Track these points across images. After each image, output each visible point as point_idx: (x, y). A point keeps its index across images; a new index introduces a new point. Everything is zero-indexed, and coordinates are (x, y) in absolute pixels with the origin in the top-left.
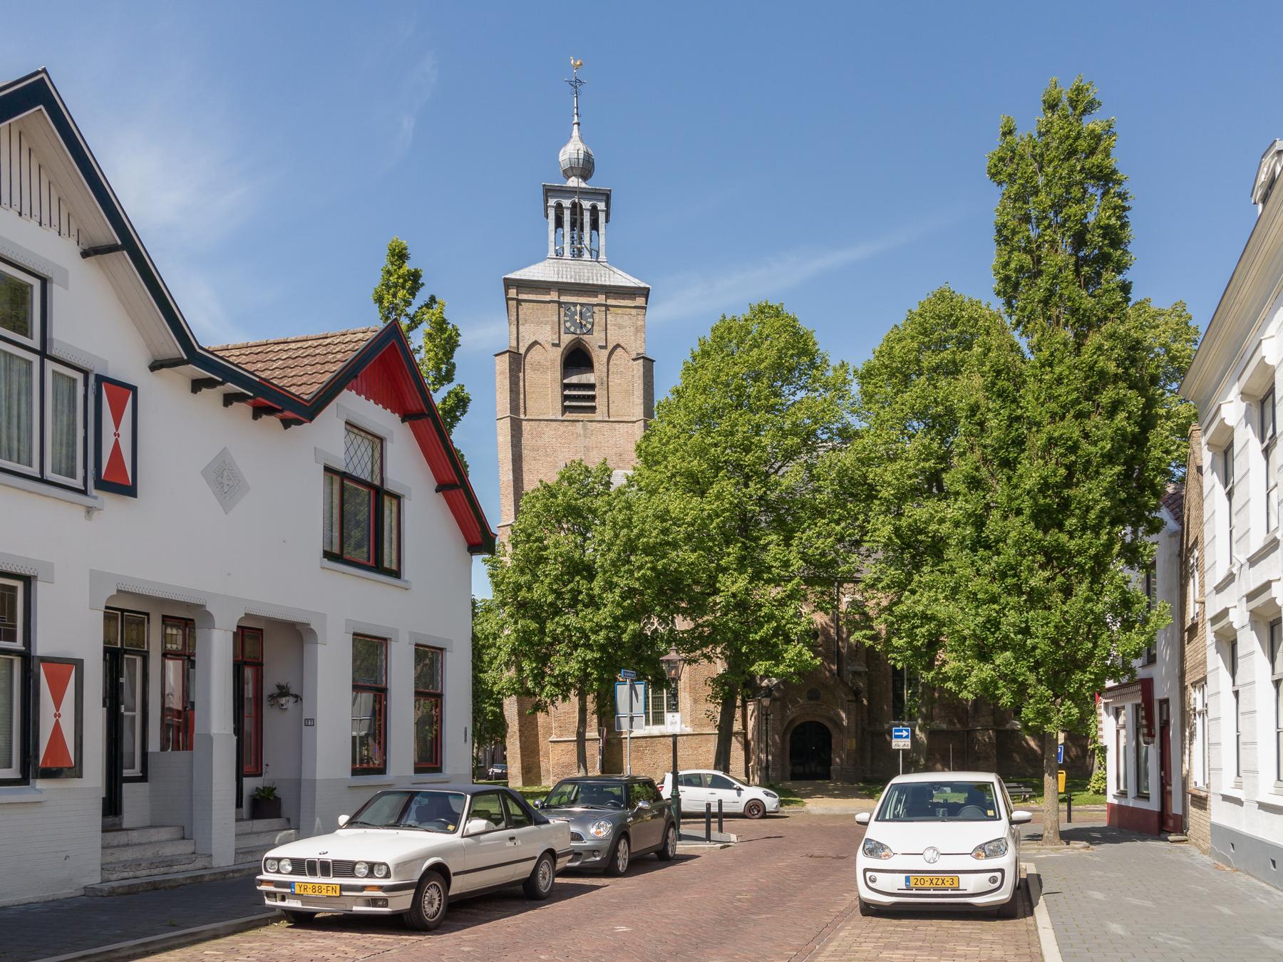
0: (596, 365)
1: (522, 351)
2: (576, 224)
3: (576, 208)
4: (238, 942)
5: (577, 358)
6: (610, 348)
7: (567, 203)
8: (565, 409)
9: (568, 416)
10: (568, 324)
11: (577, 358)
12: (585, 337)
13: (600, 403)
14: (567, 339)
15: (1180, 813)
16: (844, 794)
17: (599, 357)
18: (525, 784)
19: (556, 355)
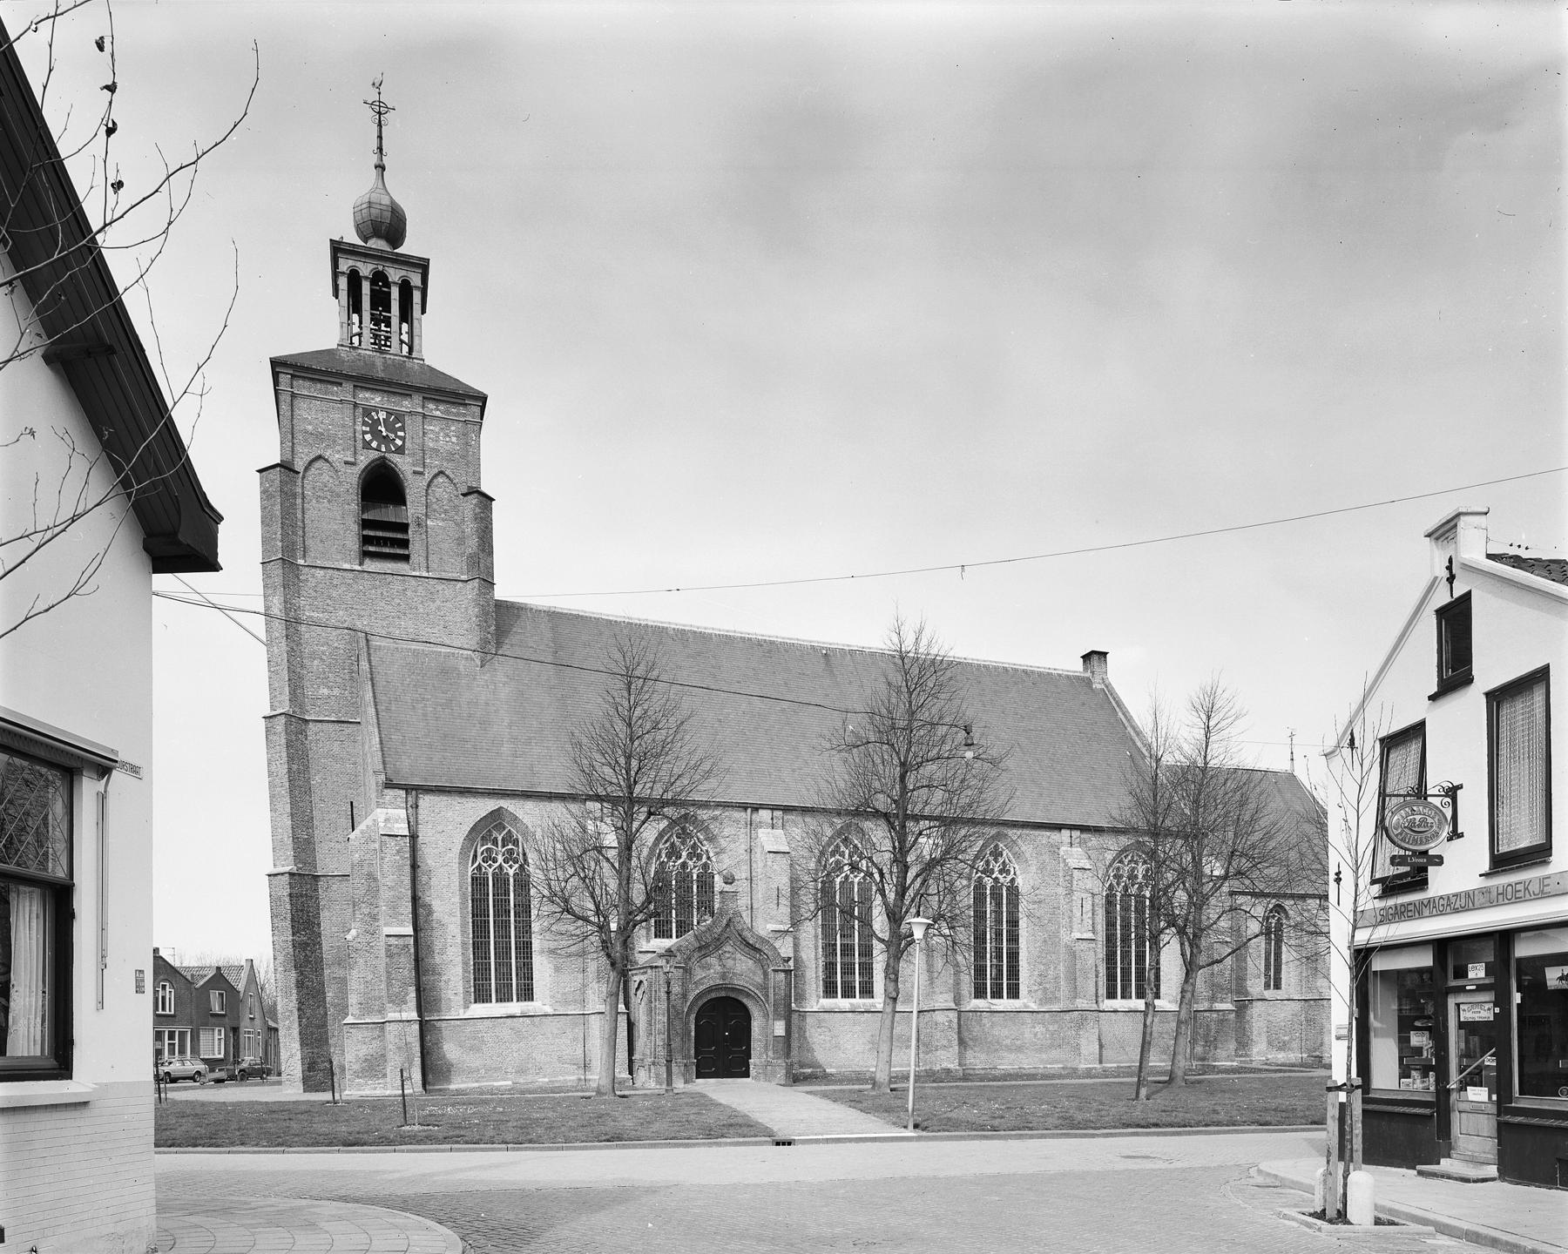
0: (409, 499)
1: (299, 465)
2: (380, 301)
3: (379, 278)
4: (1051, 941)
5: (381, 486)
6: (428, 477)
7: (366, 269)
8: (366, 554)
9: (371, 565)
10: (368, 437)
11: (381, 486)
12: (396, 459)
13: (416, 549)
14: (365, 459)
15: (61, 874)
16: (239, 1104)
17: (414, 489)
18: (1519, 960)
19: (352, 477)
